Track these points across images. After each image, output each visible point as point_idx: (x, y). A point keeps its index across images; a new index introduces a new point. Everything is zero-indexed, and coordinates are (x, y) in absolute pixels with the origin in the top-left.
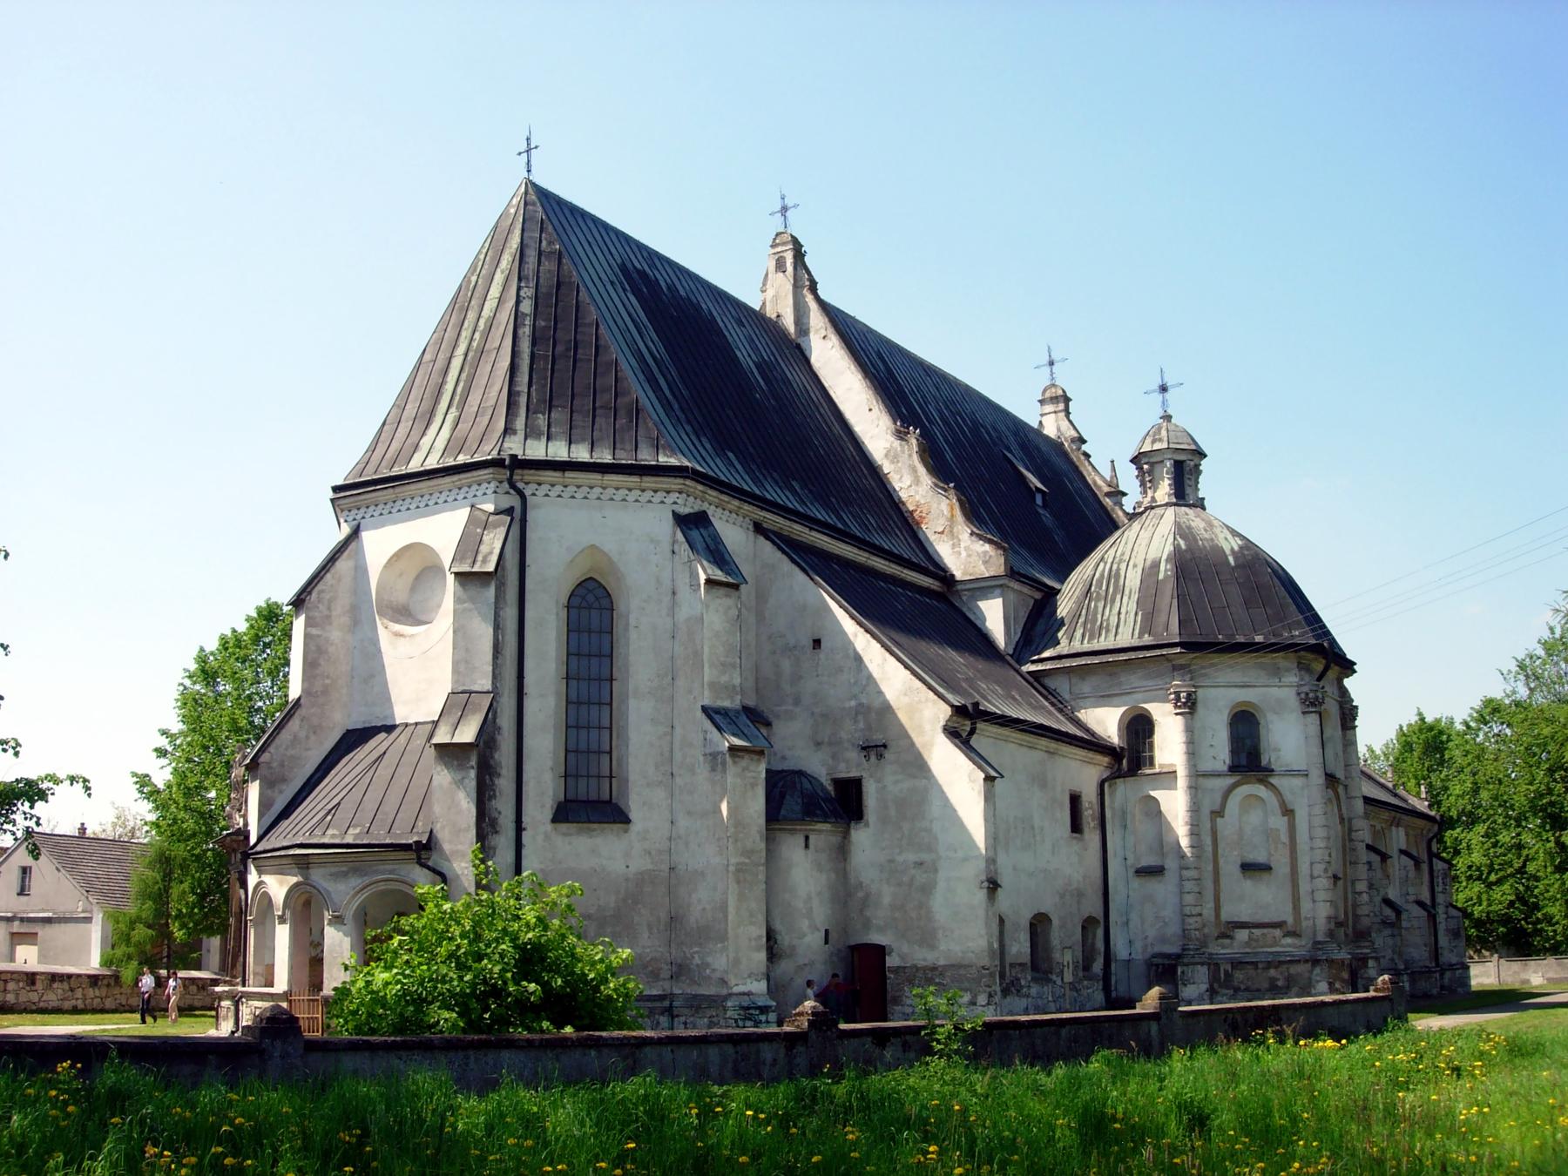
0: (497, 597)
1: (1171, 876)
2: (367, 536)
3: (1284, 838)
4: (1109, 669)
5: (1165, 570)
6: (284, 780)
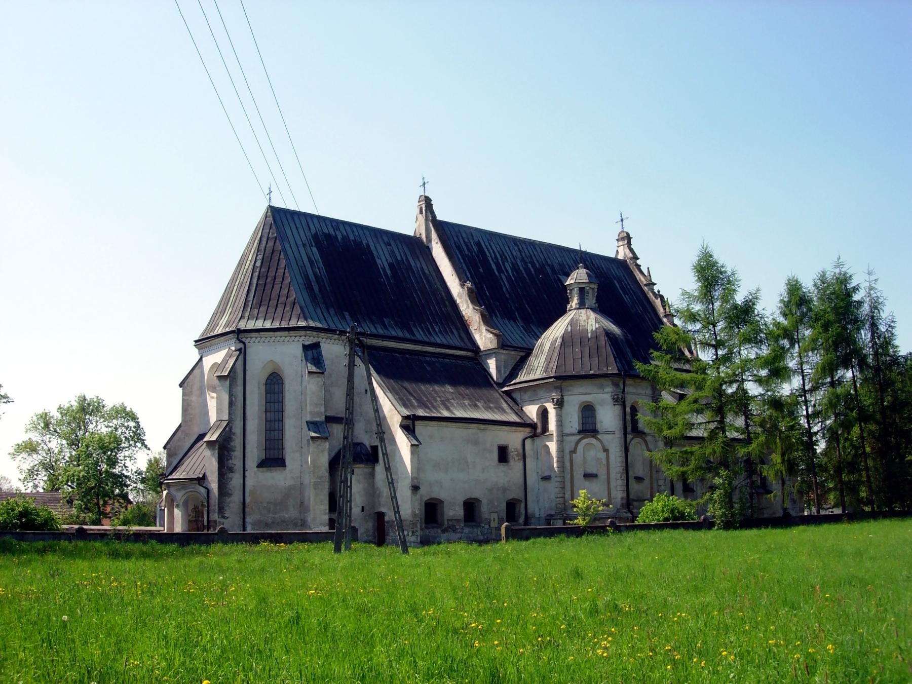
0: (230, 385)
1: (554, 479)
2: (204, 359)
3: (604, 462)
4: (535, 389)
5: (559, 340)
6: (176, 454)
